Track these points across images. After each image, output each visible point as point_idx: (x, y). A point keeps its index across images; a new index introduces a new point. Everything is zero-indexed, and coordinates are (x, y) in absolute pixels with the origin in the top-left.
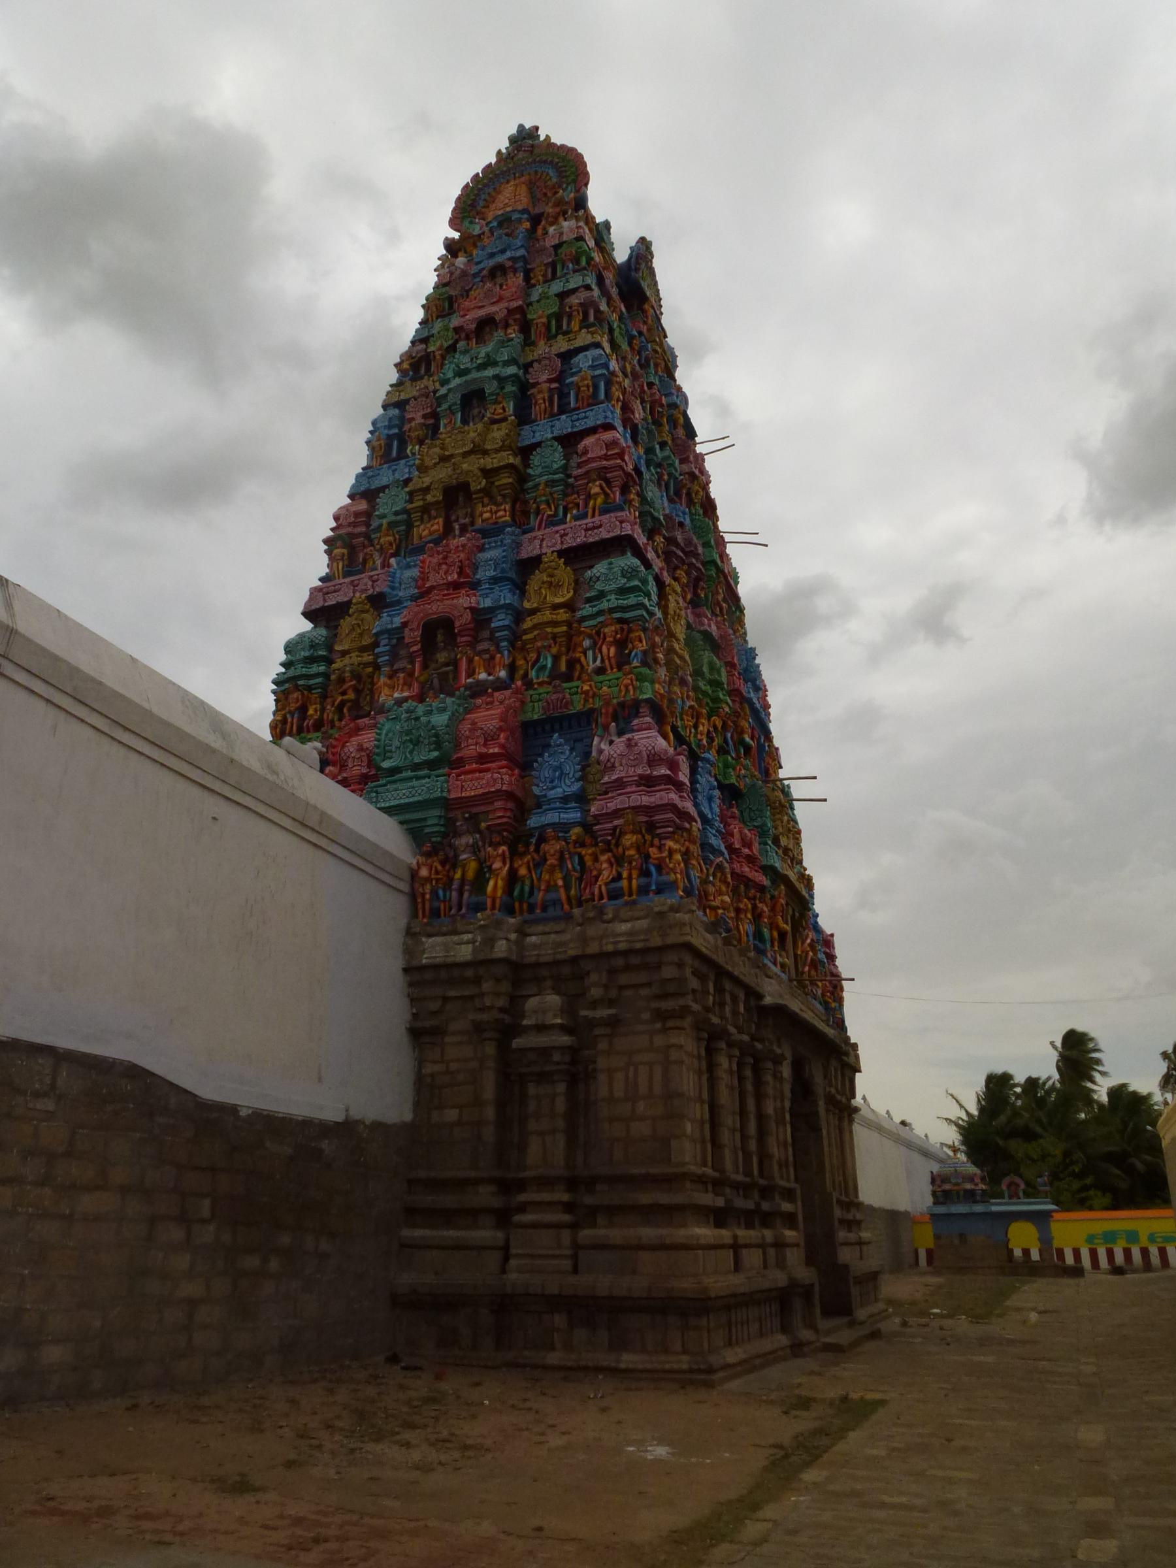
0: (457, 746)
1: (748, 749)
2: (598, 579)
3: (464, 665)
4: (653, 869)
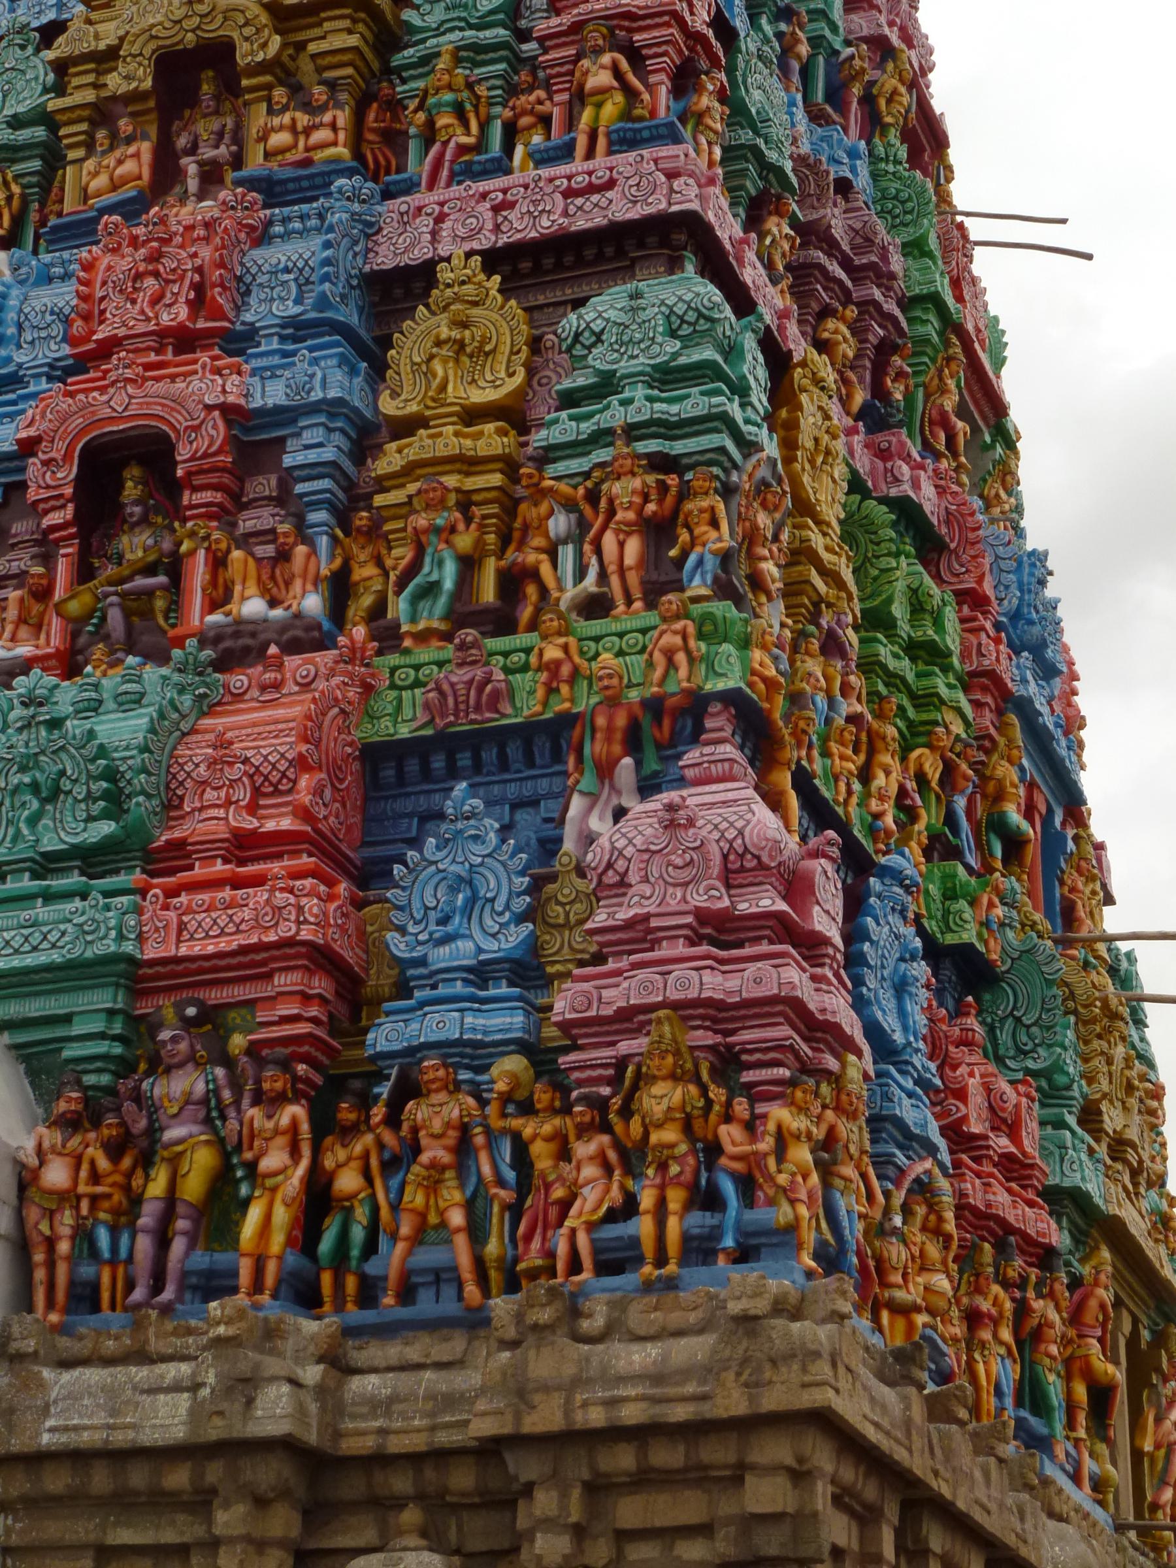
0: (171, 806)
1: (1014, 845)
2: (598, 337)
3: (198, 572)
4: (728, 1187)
